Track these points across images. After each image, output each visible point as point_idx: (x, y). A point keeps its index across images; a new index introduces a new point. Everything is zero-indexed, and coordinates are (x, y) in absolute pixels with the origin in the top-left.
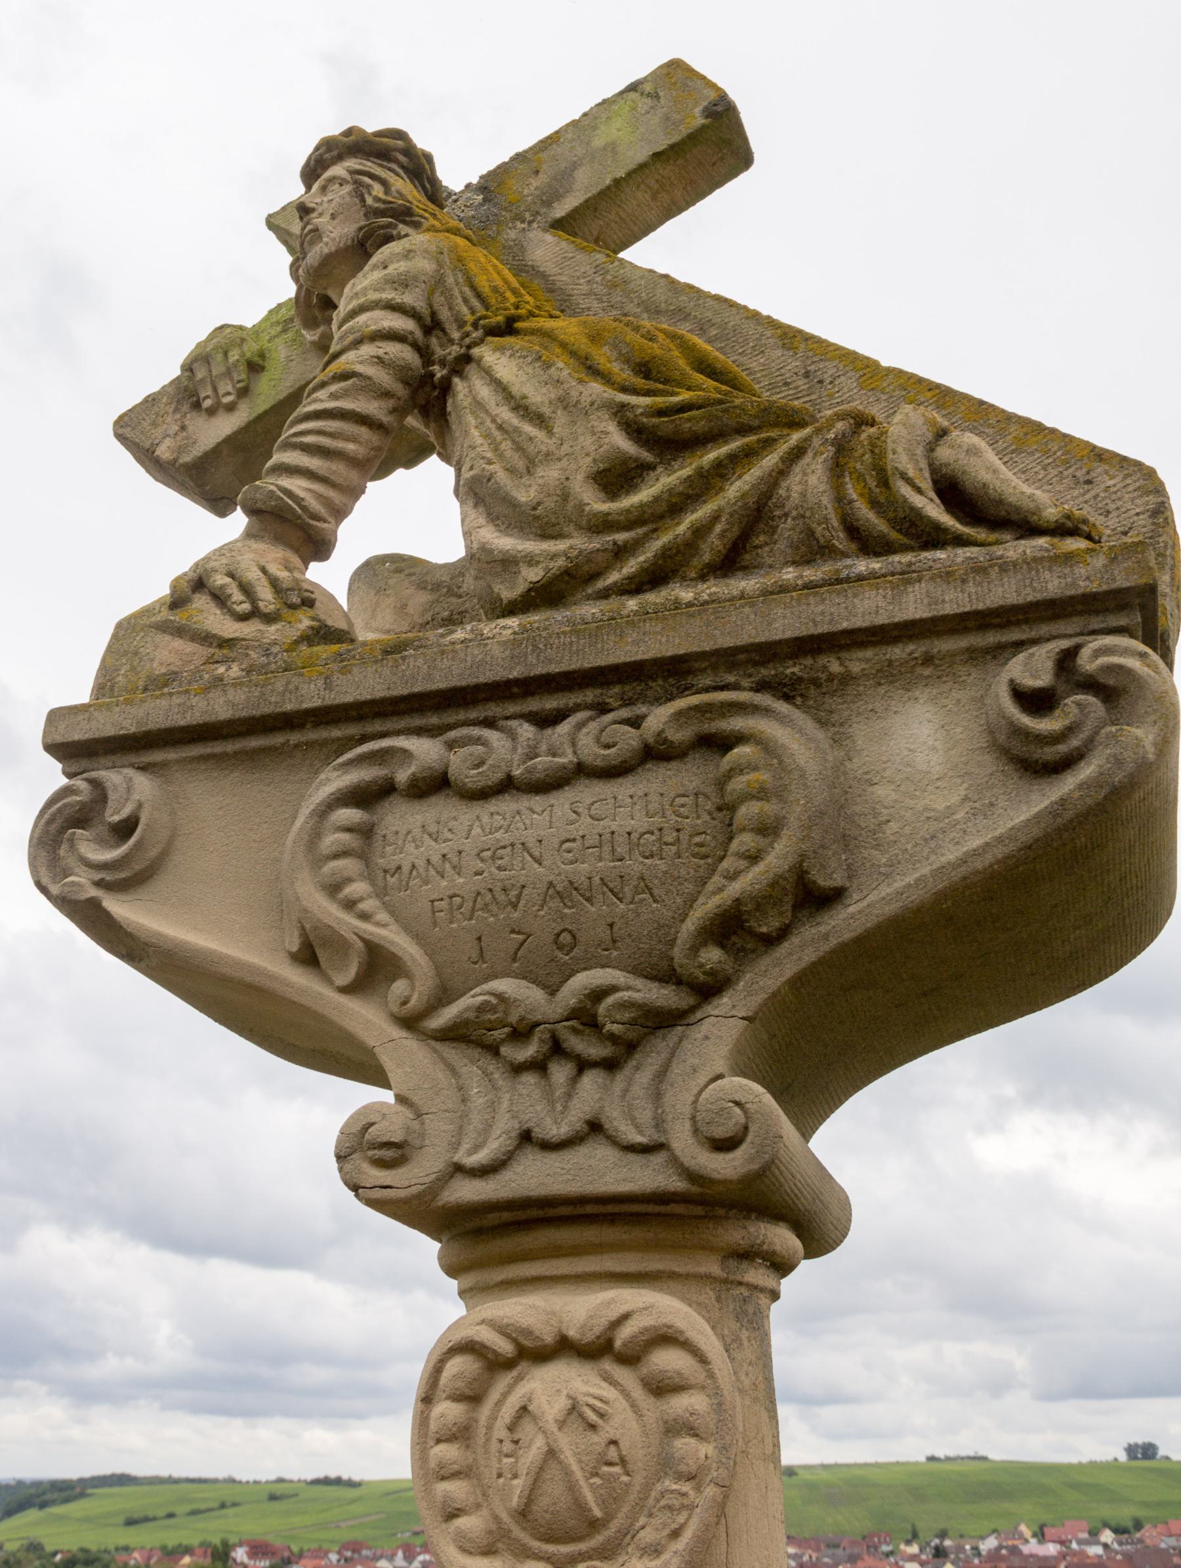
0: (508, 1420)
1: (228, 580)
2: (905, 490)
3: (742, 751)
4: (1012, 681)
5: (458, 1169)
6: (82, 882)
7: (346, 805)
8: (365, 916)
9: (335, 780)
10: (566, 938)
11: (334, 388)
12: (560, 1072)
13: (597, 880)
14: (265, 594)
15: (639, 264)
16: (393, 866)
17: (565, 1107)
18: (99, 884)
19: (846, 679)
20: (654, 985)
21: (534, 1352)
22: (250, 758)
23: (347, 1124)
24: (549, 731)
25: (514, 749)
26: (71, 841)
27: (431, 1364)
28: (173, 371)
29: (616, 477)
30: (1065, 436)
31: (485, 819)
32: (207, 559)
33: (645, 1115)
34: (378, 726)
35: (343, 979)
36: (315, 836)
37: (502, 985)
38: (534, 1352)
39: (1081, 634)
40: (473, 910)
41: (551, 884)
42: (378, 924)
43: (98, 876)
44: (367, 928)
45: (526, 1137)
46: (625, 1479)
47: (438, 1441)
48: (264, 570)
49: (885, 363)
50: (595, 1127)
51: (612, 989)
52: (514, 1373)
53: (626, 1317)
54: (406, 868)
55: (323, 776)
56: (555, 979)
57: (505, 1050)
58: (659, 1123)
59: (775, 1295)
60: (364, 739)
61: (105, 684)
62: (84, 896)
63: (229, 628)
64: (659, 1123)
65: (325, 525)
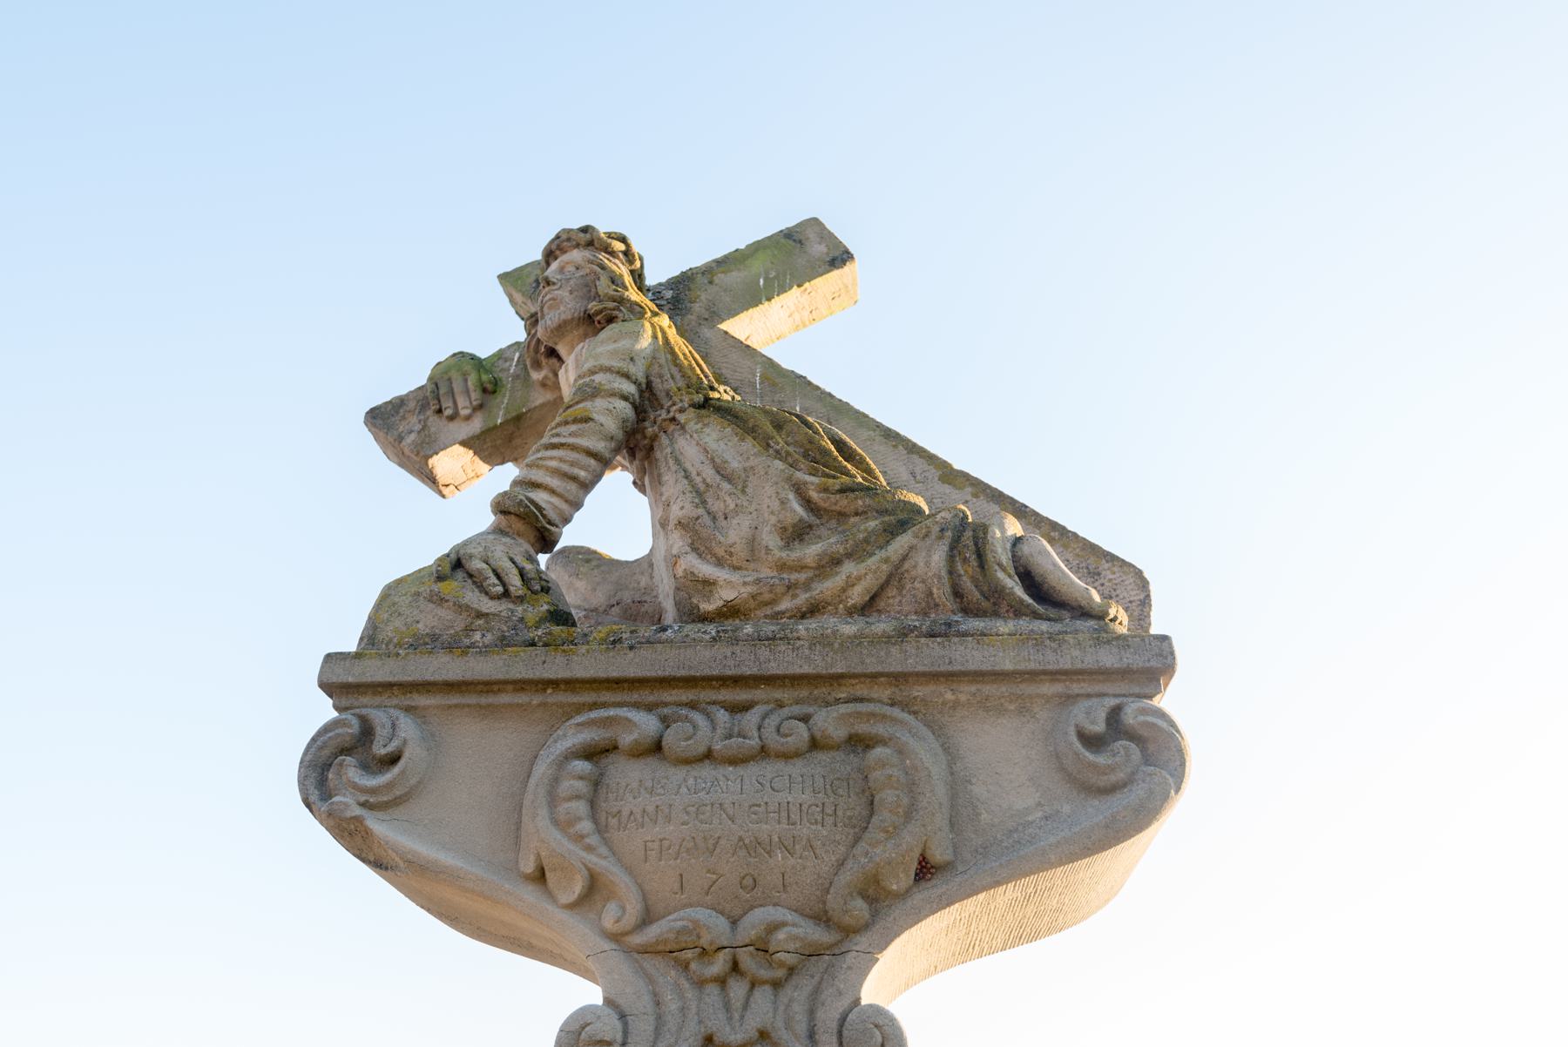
2: (1001, 575)
3: (879, 752)
8: (589, 849)
9: (573, 736)
10: (748, 881)
11: (573, 428)
12: (738, 989)
14: (515, 581)
15: (785, 365)
16: (615, 810)
17: (742, 1017)
18: (363, 805)
19: (956, 705)
20: (810, 923)
23: (566, 1023)
24: (738, 716)
28: (422, 380)
29: (797, 534)
30: (857, 412)
32: (466, 543)
34: (606, 696)
35: (568, 897)
36: (556, 781)
37: (701, 914)
41: (741, 839)
42: (600, 856)
43: (363, 799)
44: (592, 859)
48: (512, 560)
49: (956, 466)
51: (784, 924)
54: (625, 813)
55: (560, 732)
56: (737, 912)
60: (594, 706)
61: (371, 637)
62: (349, 814)
63: (488, 606)
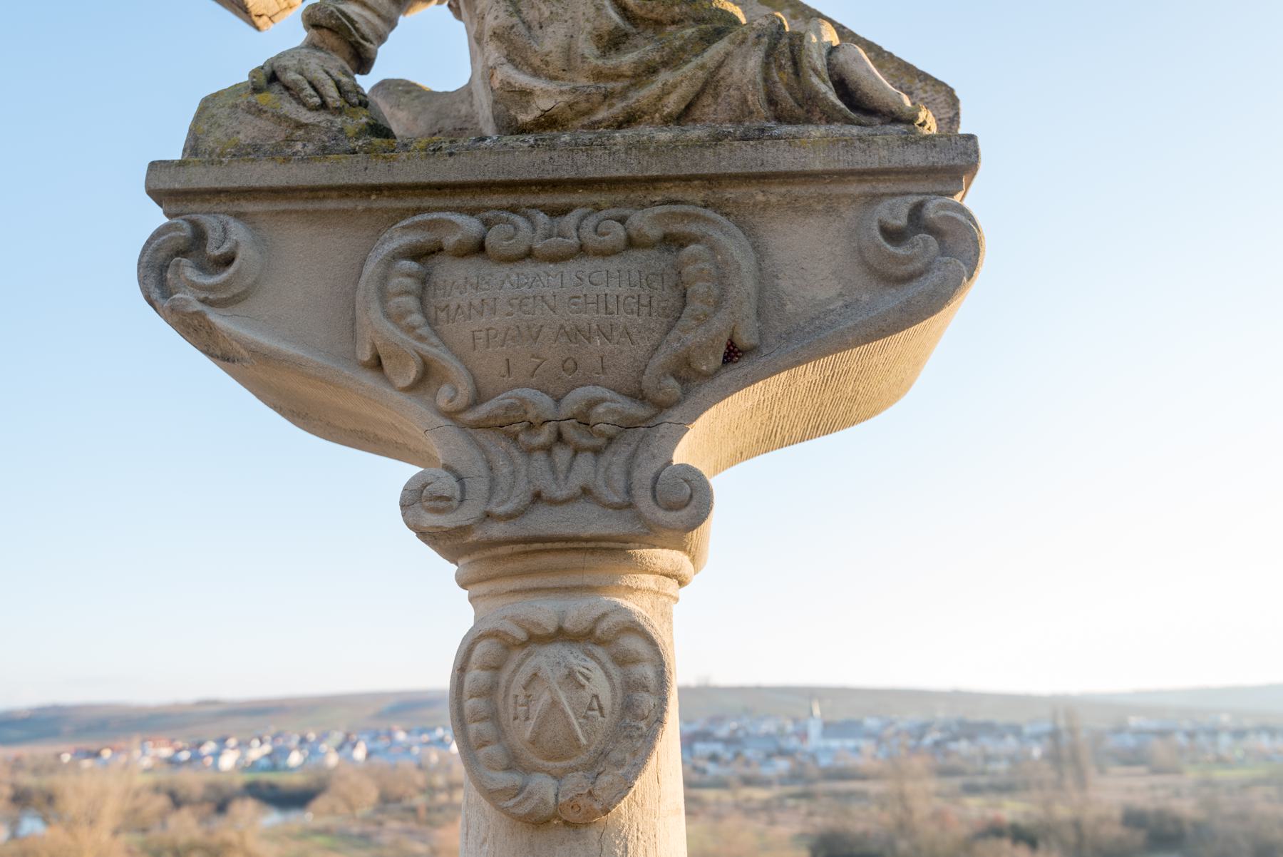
0: (523, 682)
1: (300, 77)
3: (692, 248)
4: (880, 221)
5: (488, 515)
6: (189, 299)
7: (406, 258)
8: (421, 338)
9: (398, 239)
10: (570, 364)
12: (562, 455)
13: (594, 326)
14: (332, 93)
16: (443, 304)
17: (567, 477)
18: (204, 301)
19: (766, 206)
20: (628, 400)
21: (537, 639)
22: (322, 215)
25: (534, 230)
26: (177, 265)
27: (465, 646)
29: (613, 42)
31: (514, 277)
32: (279, 57)
33: (620, 484)
34: (429, 202)
35: (403, 382)
36: (385, 279)
37: (526, 393)
38: (537, 639)
39: (927, 194)
40: (504, 340)
41: (562, 327)
42: (431, 344)
43: (202, 296)
44: (424, 347)
45: (537, 497)
46: (600, 719)
47: (471, 697)
50: (586, 492)
51: (603, 400)
52: (525, 651)
53: (604, 615)
54: (453, 307)
57: (522, 437)
58: (629, 491)
59: (677, 599)
61: (194, 146)
62: (190, 309)
63: (306, 116)
64: (629, 491)
65: (367, 44)
